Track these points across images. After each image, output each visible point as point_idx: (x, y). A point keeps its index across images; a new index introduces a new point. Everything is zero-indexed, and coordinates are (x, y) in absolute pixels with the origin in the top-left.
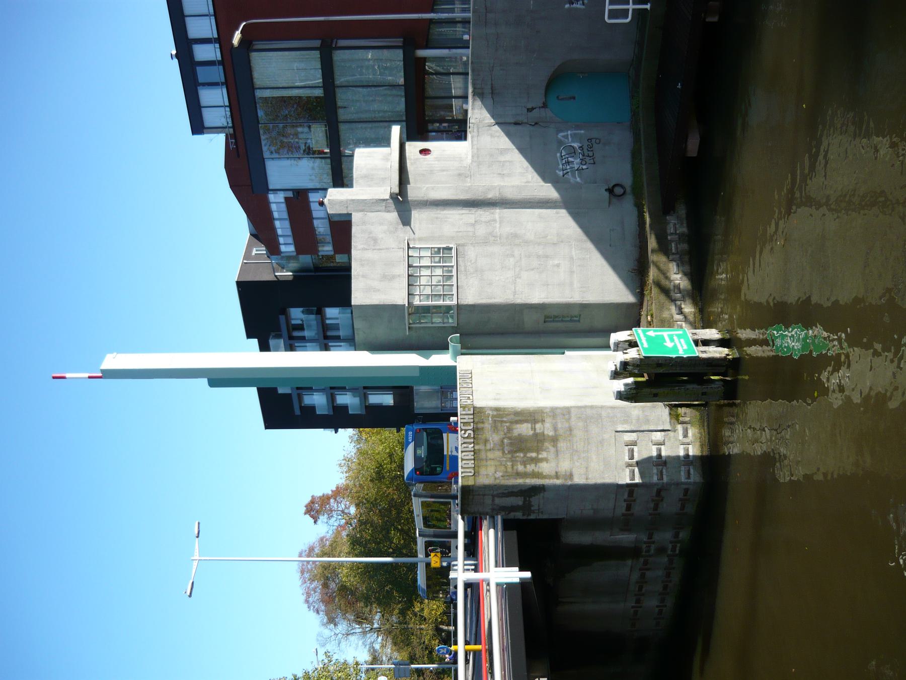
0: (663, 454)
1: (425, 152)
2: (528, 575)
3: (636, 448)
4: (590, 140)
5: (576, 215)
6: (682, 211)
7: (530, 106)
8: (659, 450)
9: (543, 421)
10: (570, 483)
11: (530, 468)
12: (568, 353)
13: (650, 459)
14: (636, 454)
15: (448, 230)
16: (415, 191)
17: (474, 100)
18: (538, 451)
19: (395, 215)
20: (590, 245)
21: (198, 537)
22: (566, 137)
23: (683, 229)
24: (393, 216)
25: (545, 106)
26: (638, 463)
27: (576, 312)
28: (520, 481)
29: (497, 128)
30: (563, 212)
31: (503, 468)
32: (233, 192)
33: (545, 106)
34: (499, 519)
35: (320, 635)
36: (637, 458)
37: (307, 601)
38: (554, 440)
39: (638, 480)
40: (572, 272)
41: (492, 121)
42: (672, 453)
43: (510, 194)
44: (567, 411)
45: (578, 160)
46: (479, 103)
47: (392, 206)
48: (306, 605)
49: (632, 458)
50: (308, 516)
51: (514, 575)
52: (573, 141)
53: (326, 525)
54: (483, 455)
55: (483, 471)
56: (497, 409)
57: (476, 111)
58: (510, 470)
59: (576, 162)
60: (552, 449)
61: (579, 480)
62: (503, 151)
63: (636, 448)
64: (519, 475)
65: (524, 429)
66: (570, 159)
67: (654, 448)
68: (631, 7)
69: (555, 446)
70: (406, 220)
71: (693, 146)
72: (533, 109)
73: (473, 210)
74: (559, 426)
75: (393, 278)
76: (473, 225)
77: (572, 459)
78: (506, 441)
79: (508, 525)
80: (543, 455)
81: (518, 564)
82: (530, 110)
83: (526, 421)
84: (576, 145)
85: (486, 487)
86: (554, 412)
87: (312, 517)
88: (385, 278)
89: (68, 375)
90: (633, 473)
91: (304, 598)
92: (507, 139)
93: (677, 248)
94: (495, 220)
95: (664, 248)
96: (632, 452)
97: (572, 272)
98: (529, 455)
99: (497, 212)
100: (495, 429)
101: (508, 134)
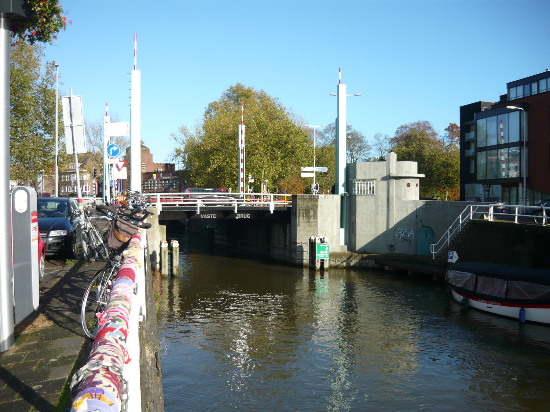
0: (304, 253)
1: (417, 185)
2: (272, 212)
3: (306, 245)
4: (410, 240)
5: (384, 234)
6: (376, 266)
7: (422, 221)
8: (305, 252)
9: (314, 219)
10: (297, 225)
11: (301, 214)
12: (343, 231)
13: (303, 249)
14: (304, 245)
15: (380, 193)
16: (393, 182)
17: (425, 202)
18: (306, 217)
19: (385, 175)
20: (374, 237)
21: (355, 95)
22: (412, 232)
23: (370, 265)
24: (385, 175)
25: (423, 226)
26: (302, 245)
27: (354, 233)
28: (298, 212)
29: (415, 209)
30: (385, 230)
31: (301, 207)
32: (471, 104)
33: (423, 226)
34: (291, 206)
35: (381, 135)
36: (303, 245)
37: (402, 127)
38: (309, 222)
39: (298, 245)
40: (366, 232)
41: (418, 208)
42: (304, 256)
43: (391, 212)
44: (317, 226)
45: (403, 236)
46: (424, 203)
47: (388, 175)
48: (400, 126)
49: (304, 244)
50: (449, 125)
51: (272, 209)
52: (410, 235)
53: (444, 135)
54: (305, 201)
55: (300, 201)
56: (317, 206)
57: (421, 202)
58: (301, 209)
59: (403, 235)
60: (306, 221)
61: (298, 228)
62: (407, 211)
63: (306, 245)
64: (299, 211)
65: (312, 213)
66: (403, 233)
67: (306, 250)
68: (434, 252)
69: (307, 222)
70: (383, 179)
71: (386, 268)
72: (422, 222)
73: (386, 201)
74: (312, 223)
75: (365, 175)
76: (382, 201)
77: (303, 226)
78: (309, 208)
79: (289, 208)
80: (305, 218)
81: (276, 210)
82: (421, 221)
83: (314, 214)
84: (408, 235)
85: (296, 202)
86: (316, 222)
87: (449, 128)
88: (365, 172)
89: (340, 72)
90: (300, 244)
91: (404, 125)
92: (411, 212)
93: (364, 263)
94: (383, 207)
95: (363, 259)
96: (305, 244)
97: (366, 232)
98: (305, 214)
99: (386, 209)
100: (312, 205)
101: (413, 213)
